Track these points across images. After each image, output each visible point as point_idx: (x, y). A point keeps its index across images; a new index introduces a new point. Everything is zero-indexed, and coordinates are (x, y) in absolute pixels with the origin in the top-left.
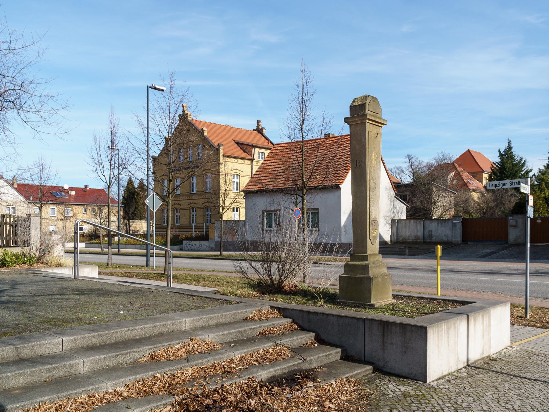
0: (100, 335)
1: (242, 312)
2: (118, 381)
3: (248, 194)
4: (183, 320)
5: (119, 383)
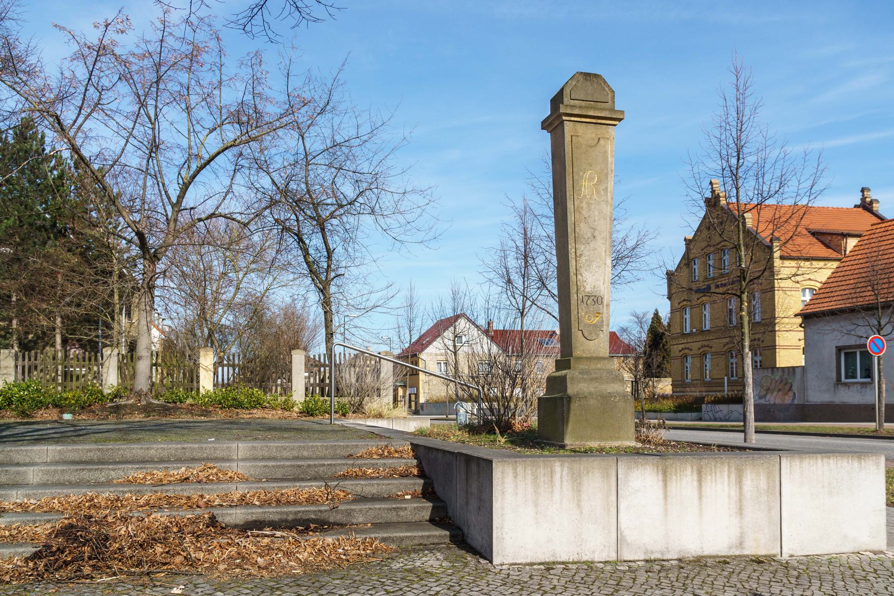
0: (99, 450)
1: (348, 446)
2: (35, 491)
3: (808, 318)
4: (234, 445)
5: (35, 494)
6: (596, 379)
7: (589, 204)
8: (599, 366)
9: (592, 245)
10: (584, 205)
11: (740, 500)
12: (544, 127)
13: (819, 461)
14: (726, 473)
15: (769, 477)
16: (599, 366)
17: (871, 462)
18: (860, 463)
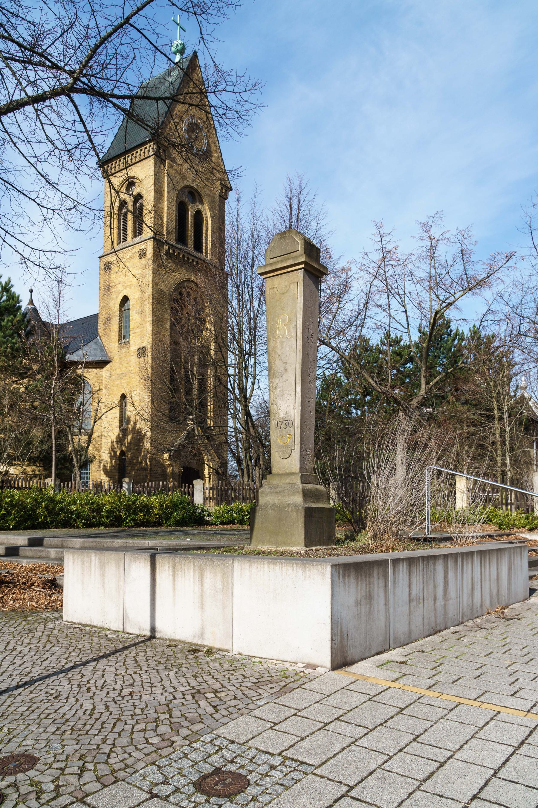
6: (279, 492)
7: (282, 343)
8: (288, 481)
9: (284, 377)
10: (278, 345)
11: (202, 596)
13: (266, 566)
14: (192, 571)
15: (223, 578)
16: (288, 481)
17: (316, 572)
18: (305, 571)
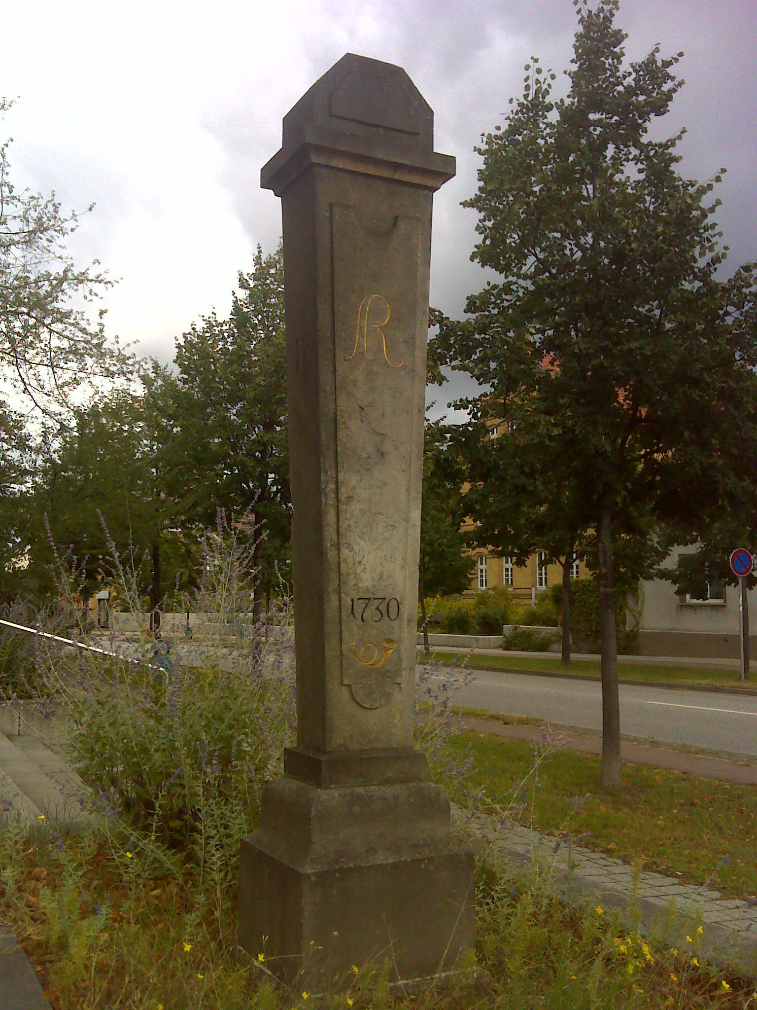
12: (575, 35)
